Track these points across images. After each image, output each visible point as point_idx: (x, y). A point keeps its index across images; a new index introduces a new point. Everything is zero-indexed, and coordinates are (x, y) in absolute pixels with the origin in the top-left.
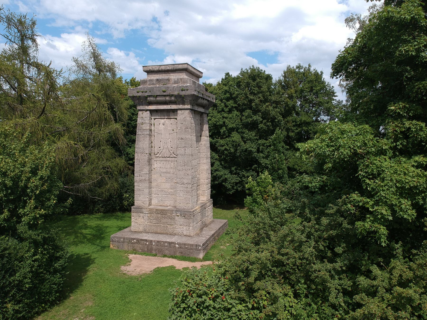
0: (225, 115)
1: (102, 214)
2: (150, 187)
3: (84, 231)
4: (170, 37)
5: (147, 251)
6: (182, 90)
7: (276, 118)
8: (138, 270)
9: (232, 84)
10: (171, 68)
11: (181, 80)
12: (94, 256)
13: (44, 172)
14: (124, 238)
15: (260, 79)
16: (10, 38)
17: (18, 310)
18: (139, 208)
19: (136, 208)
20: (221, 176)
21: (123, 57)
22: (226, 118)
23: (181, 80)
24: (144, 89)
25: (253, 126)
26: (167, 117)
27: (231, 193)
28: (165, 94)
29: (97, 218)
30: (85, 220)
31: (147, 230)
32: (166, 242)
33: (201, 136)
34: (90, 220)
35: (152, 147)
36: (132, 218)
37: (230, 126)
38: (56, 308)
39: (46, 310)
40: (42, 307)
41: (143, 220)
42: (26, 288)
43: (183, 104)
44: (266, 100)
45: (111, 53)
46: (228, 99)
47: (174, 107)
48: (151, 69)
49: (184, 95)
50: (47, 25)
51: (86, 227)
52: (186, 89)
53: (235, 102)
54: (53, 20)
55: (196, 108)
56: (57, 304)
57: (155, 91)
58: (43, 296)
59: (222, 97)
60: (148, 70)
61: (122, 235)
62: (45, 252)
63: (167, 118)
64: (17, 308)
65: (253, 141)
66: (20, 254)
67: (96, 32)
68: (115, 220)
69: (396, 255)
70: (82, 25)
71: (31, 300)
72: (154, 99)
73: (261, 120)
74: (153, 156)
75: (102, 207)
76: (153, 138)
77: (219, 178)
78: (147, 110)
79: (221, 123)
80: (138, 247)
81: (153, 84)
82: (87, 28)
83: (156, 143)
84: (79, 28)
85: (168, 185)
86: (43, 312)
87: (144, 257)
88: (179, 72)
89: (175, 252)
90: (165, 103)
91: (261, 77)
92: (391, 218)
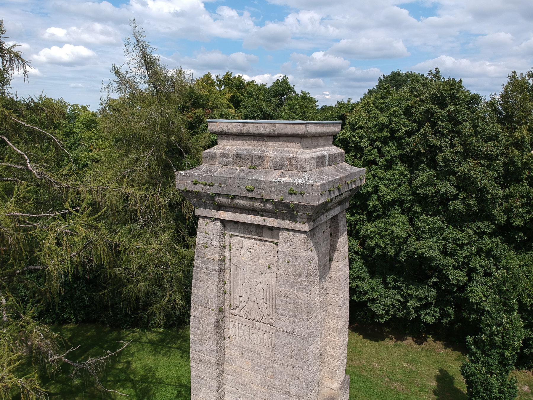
0: (379, 173)
2: (220, 375)
6: (291, 194)
7: (488, 192)
9: (395, 112)
10: (267, 131)
11: (290, 161)
15: (455, 104)
21: (236, 18)
23: (290, 161)
25: (438, 204)
26: (256, 237)
27: (382, 321)
28: (250, 195)
33: (330, 260)
35: (225, 293)
43: (293, 218)
47: (271, 222)
49: (295, 205)
52: (300, 190)
53: (400, 146)
57: (230, 186)
59: (375, 136)
60: (220, 130)
65: (435, 233)
72: (229, 201)
73: (455, 192)
74: (227, 312)
76: (227, 276)
78: (215, 219)
79: (370, 190)
81: (229, 164)
83: (232, 285)
88: (285, 139)
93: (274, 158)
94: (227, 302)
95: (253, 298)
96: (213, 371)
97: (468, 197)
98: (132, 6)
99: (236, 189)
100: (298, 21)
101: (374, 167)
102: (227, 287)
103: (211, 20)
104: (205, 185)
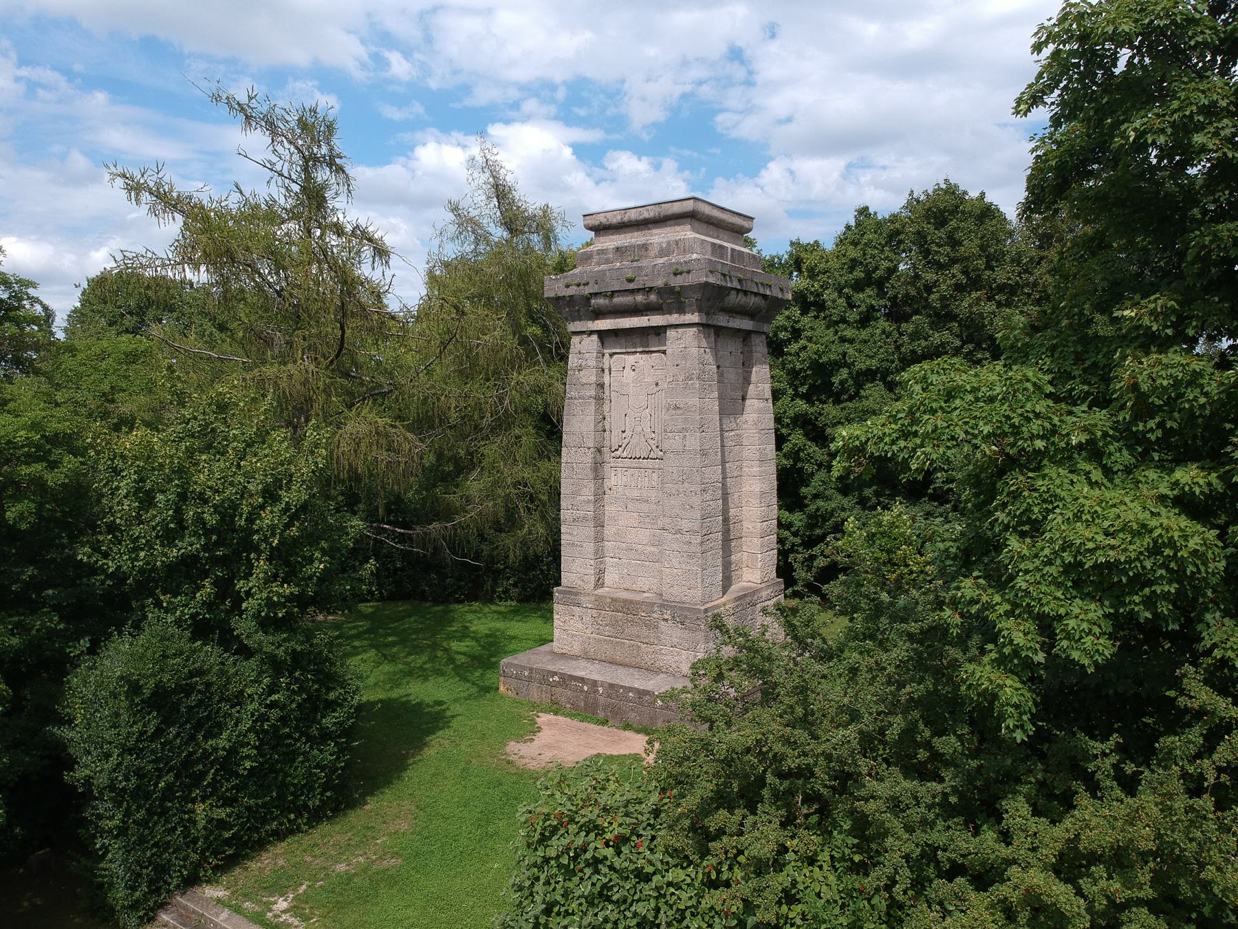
1: (514, 603)
2: (599, 539)
3: (455, 645)
4: (779, 103)
5: (586, 710)
6: (675, 274)
8: (548, 755)
9: (870, 241)
10: (652, 214)
12: (457, 708)
13: (293, 496)
14: (531, 670)
16: (278, 168)
17: (221, 821)
18: (570, 593)
19: (564, 592)
20: (832, 515)
21: (646, 175)
22: (851, 341)
24: (582, 277)
28: (632, 286)
29: (500, 613)
30: (469, 617)
31: (591, 654)
32: (631, 689)
33: (744, 399)
34: (479, 619)
36: (556, 617)
37: (861, 365)
38: (325, 827)
39: (299, 830)
40: (290, 821)
41: (580, 626)
42: (245, 769)
43: (681, 310)
44: (975, 283)
45: (614, 166)
46: (859, 286)
47: (657, 320)
48: (604, 221)
50: (451, 105)
51: (464, 634)
53: (881, 294)
54: (466, 89)
55: (722, 320)
56: (329, 818)
58: (292, 794)
61: (530, 659)
62: (295, 687)
63: (641, 352)
64: (221, 813)
66: (233, 688)
67: (576, 110)
68: (539, 621)
69: (1094, 773)
70: (538, 96)
71: (260, 801)
72: (607, 301)
73: (958, 343)
74: (607, 456)
75: (515, 585)
76: (606, 407)
77: (825, 520)
78: (591, 333)
80: (564, 695)
81: (608, 261)
82: (553, 101)
83: (615, 421)
84: (530, 105)
85: (643, 535)
86: (291, 832)
87: (576, 723)
89: (653, 719)
90: (636, 312)
91: (963, 212)
92: (1040, 657)
93: (660, 244)
94: (607, 443)
95: (639, 429)
96: (589, 530)
97: (975, 350)
98: (417, 159)
99: (614, 282)
100: (791, 172)
101: (842, 326)
102: (607, 423)
103: (590, 183)
104: (579, 285)
